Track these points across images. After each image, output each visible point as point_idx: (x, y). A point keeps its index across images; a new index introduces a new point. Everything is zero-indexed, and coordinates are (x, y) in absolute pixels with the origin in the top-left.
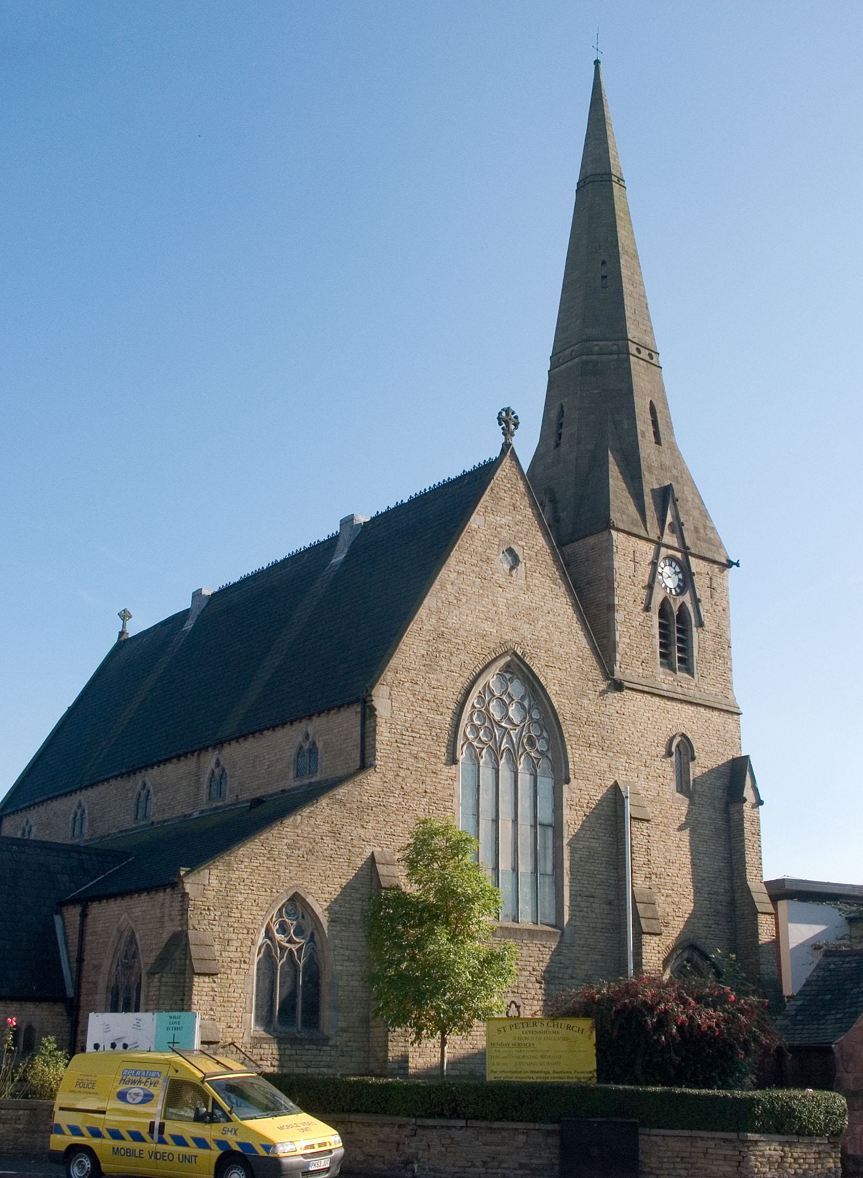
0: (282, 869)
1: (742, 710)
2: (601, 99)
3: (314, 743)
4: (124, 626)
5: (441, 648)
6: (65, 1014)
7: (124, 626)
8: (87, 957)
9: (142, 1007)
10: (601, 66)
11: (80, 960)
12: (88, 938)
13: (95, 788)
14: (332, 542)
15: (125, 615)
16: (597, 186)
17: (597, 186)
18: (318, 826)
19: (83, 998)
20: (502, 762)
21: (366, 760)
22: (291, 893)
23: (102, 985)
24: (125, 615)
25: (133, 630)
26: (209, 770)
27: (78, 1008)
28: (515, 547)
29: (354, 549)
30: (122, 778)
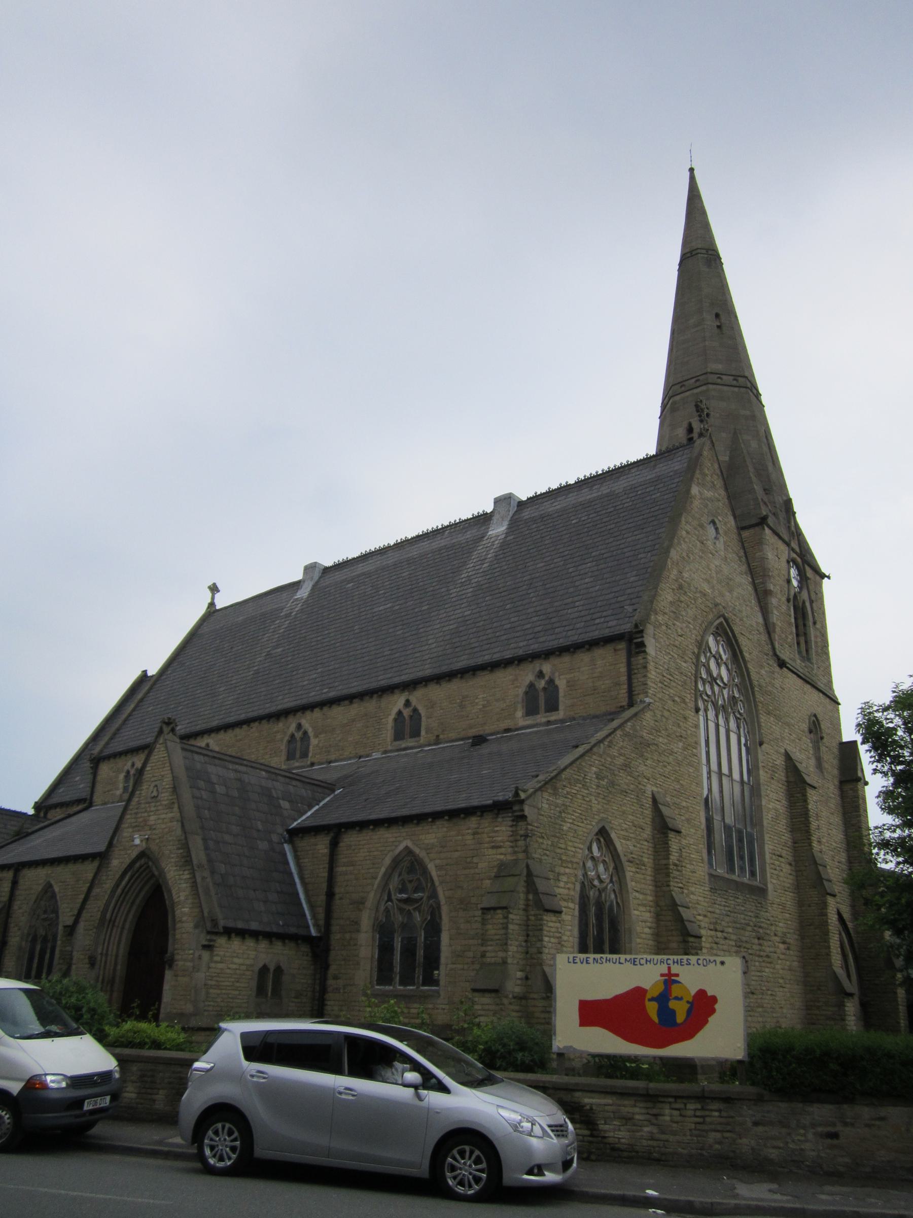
0: (593, 798)
1: (840, 701)
2: (699, 197)
3: (551, 681)
4: (213, 598)
5: (682, 599)
6: (310, 954)
7: (213, 598)
8: (337, 890)
9: (607, 946)
10: (695, 172)
11: (330, 895)
12: (340, 869)
13: (230, 731)
14: (483, 520)
15: (214, 589)
16: (700, 263)
17: (700, 263)
18: (613, 757)
19: (335, 937)
20: (720, 717)
21: (635, 697)
22: (600, 826)
23: (366, 921)
24: (214, 589)
25: (222, 602)
26: (395, 711)
27: (327, 950)
28: (716, 520)
29: (514, 524)
30: (268, 721)
